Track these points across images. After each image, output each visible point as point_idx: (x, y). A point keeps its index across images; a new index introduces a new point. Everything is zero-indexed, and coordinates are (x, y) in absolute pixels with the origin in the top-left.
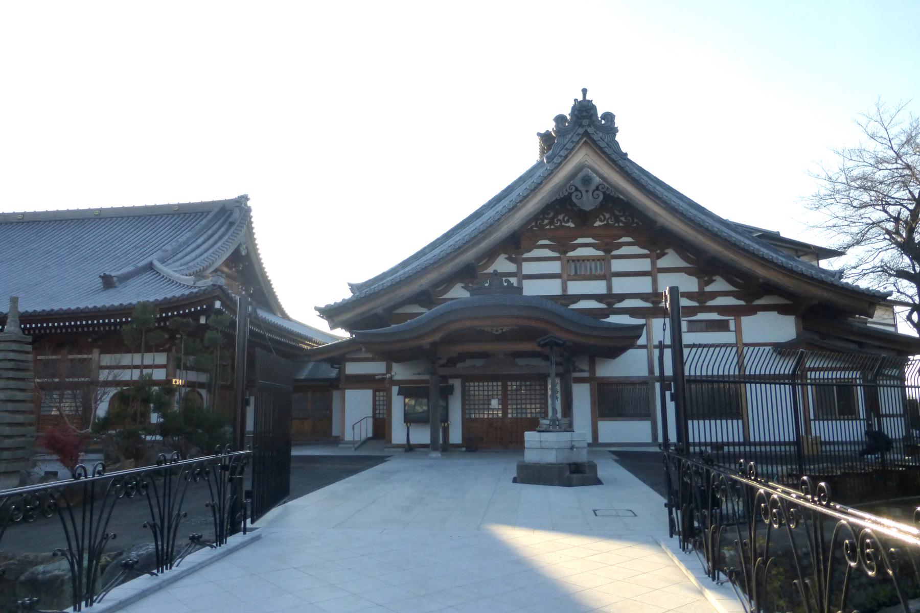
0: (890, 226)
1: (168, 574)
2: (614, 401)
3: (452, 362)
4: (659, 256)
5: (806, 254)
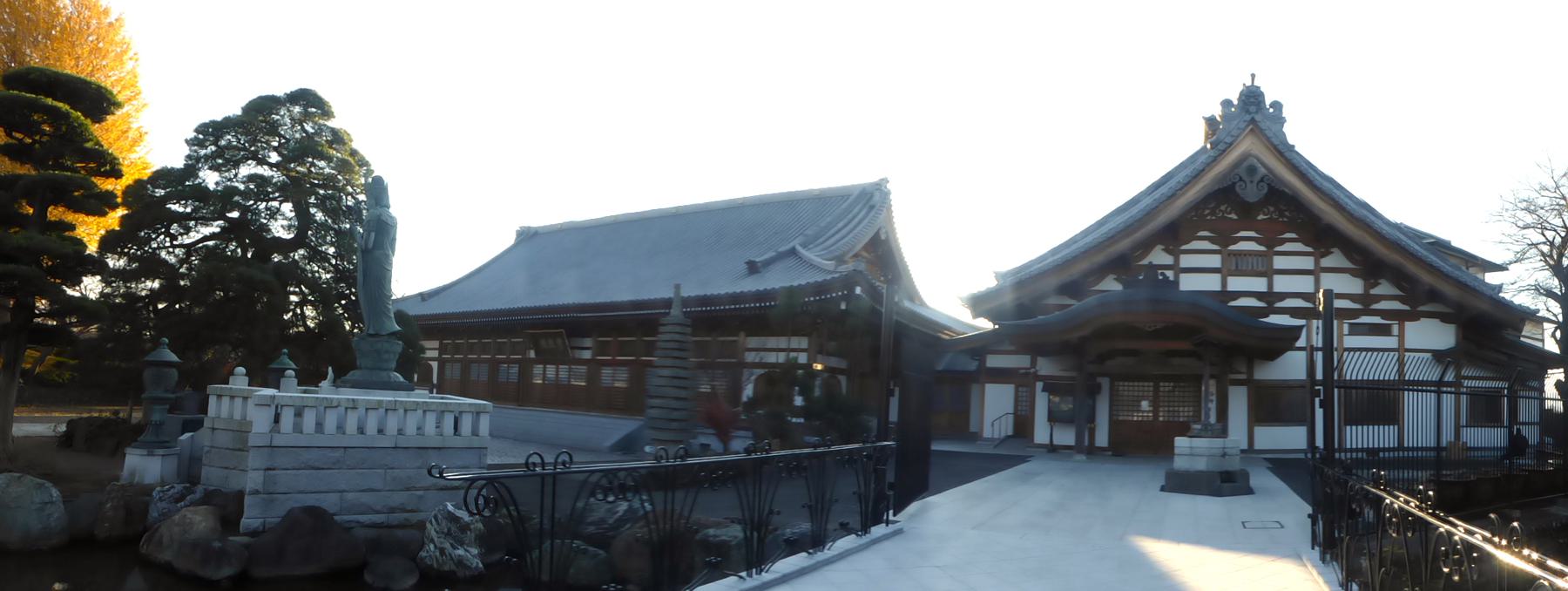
0: (1546, 249)
1: (820, 556)
2: (1272, 405)
3: (1102, 358)
4: (1323, 256)
5: (1475, 265)
